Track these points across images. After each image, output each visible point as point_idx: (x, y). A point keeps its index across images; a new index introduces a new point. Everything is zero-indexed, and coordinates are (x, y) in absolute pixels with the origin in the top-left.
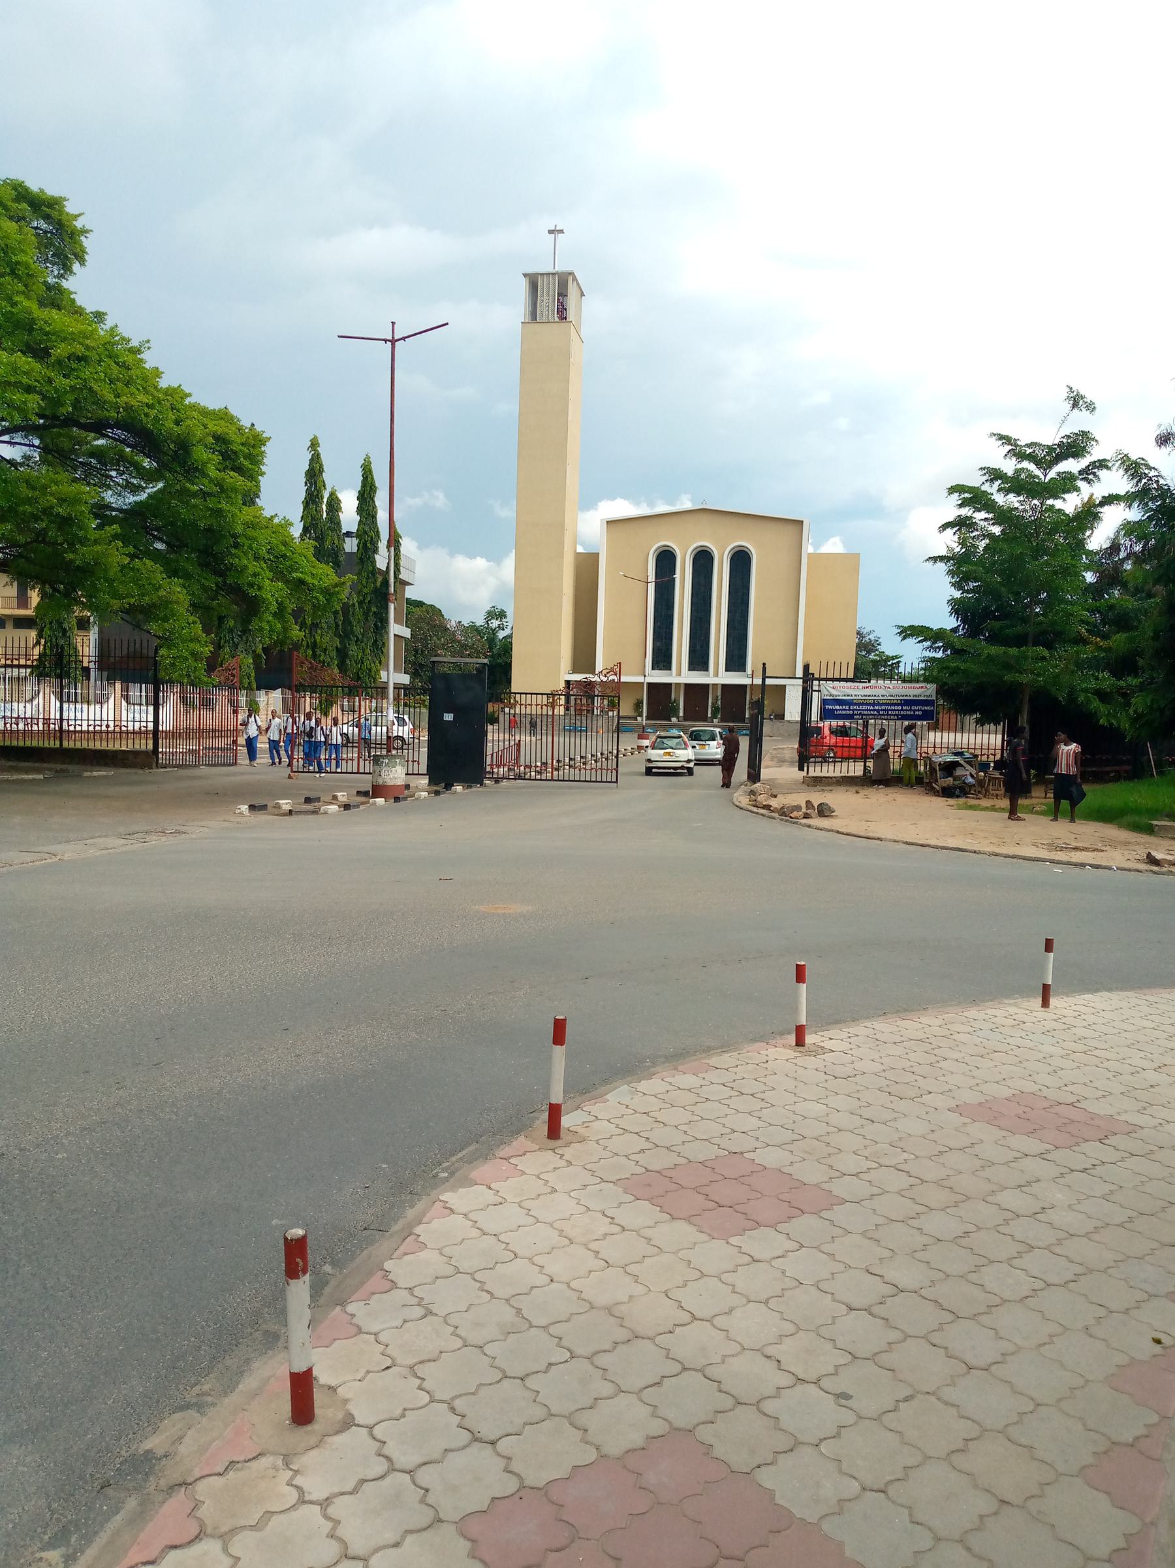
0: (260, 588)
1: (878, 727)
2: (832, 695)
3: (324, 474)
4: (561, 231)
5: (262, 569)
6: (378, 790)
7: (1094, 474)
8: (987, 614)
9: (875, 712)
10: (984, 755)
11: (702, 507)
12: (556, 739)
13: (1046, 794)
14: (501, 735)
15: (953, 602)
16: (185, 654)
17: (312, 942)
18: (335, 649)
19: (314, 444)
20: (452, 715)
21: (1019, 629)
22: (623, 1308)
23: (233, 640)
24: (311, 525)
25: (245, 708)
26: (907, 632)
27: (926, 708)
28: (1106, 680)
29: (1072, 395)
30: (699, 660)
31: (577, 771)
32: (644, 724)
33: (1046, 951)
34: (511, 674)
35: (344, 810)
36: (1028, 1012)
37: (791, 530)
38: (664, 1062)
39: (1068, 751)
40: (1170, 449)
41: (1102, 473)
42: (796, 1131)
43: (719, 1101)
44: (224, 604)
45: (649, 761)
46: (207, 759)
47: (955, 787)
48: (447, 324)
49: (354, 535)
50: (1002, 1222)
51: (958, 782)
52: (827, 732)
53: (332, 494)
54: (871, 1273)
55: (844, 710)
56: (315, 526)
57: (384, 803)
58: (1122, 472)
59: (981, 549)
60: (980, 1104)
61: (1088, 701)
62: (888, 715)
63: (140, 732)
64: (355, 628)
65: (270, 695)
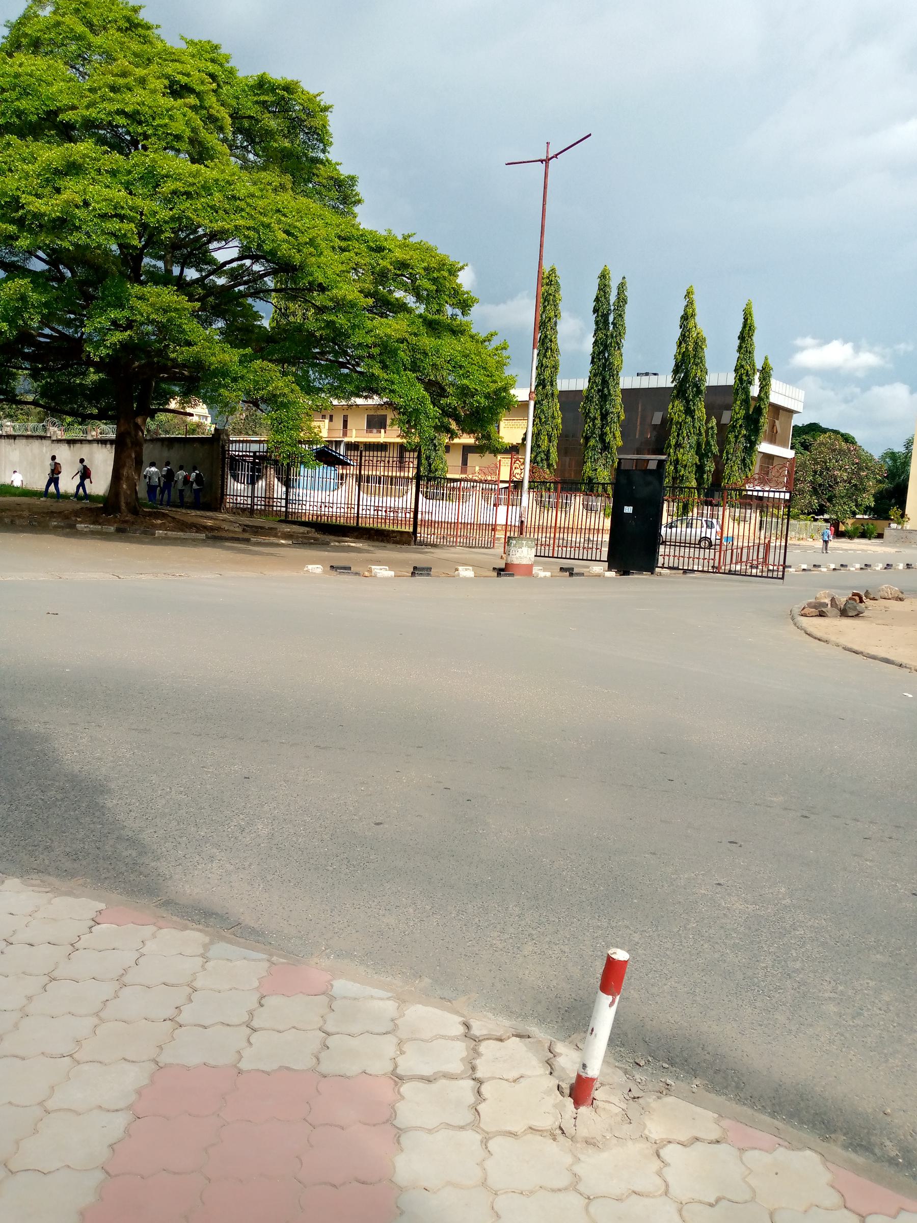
20: (632, 507)
48: (590, 135)
64: (713, 447)
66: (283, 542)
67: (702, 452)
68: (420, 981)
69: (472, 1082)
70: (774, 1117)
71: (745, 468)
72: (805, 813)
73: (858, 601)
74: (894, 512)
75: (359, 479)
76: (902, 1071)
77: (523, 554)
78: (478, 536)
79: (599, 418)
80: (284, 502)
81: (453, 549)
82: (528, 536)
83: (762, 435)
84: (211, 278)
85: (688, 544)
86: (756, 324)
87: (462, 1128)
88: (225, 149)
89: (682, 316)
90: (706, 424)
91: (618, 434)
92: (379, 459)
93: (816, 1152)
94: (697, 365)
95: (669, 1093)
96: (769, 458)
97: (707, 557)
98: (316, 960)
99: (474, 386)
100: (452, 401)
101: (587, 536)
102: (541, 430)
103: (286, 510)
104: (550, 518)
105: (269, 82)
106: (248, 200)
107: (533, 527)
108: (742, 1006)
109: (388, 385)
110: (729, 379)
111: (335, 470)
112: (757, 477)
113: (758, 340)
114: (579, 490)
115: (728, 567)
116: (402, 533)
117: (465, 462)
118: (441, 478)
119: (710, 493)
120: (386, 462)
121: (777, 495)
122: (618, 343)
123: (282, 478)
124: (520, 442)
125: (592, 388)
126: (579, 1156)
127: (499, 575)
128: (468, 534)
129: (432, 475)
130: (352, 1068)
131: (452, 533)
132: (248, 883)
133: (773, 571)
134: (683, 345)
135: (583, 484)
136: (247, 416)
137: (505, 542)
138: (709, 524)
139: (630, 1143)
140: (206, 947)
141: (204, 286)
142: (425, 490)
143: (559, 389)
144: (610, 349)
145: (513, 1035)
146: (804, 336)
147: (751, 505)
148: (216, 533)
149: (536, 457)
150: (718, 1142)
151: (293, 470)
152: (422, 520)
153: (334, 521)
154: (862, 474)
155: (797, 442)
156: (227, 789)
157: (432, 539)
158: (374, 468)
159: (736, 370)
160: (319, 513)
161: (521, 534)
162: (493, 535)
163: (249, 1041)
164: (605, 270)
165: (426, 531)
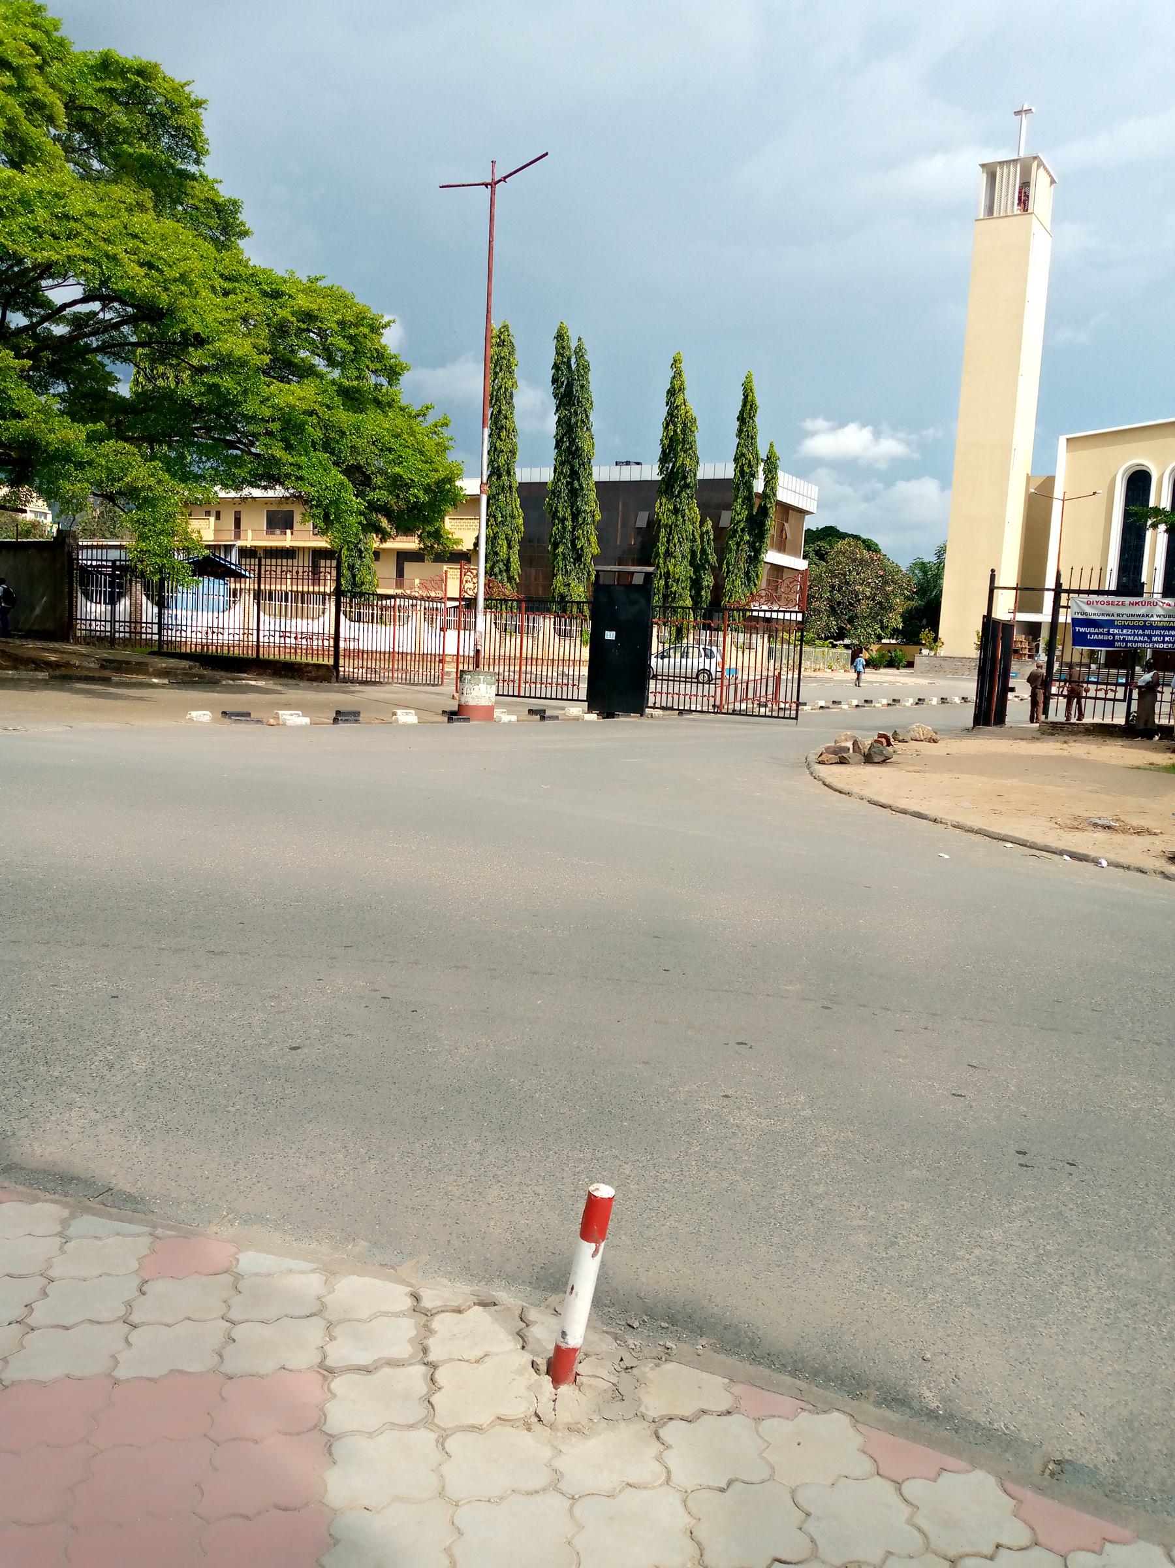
19: (676, 362)
55: (1101, 634)
66: (155, 680)
67: (697, 563)
68: (354, 1246)
69: (423, 1368)
70: (796, 1377)
71: (749, 582)
72: (826, 1004)
73: (885, 744)
74: (926, 635)
75: (258, 595)
76: (943, 1307)
77: (481, 693)
78: (421, 670)
79: (570, 518)
80: (156, 627)
81: (388, 688)
82: (486, 668)
83: (768, 541)
84: (45, 325)
85: (686, 679)
86: (758, 402)
87: (411, 1426)
88: (58, 149)
89: (669, 390)
90: (700, 527)
91: (593, 539)
92: (284, 568)
93: (844, 1412)
94: (685, 452)
95: (670, 1358)
96: (778, 569)
97: (706, 693)
98: (216, 1229)
99: (409, 476)
100: (380, 495)
101: (561, 668)
102: (497, 532)
103: (160, 638)
104: (513, 647)
105: (117, 62)
106: (87, 220)
107: (492, 657)
108: (755, 1244)
109: (293, 470)
110: (728, 471)
111: (225, 584)
112: (763, 593)
113: (761, 420)
114: (549, 611)
115: (731, 707)
116: (318, 667)
117: (400, 573)
118: (369, 594)
119: (708, 615)
120: (294, 573)
121: (787, 616)
122: (583, 421)
123: (153, 595)
124: (471, 547)
125: (559, 480)
126: (561, 1447)
127: (450, 720)
128: (409, 668)
129: (358, 590)
130: (267, 1365)
131: (387, 666)
132: (121, 1136)
133: (785, 709)
134: (671, 427)
135: (554, 602)
136: (102, 513)
137: (457, 678)
138: (708, 652)
139: (623, 1424)
140: (65, 1223)
141: (35, 337)
142: (348, 609)
143: (519, 480)
144: (576, 431)
145: (475, 1304)
146: (814, 416)
147: (757, 628)
148: (63, 671)
149: (492, 568)
150: (729, 1413)
151: (168, 584)
152: (345, 650)
153: (226, 652)
154: (887, 589)
155: (810, 549)
156: (88, 1012)
157: (361, 673)
158: (279, 580)
159: (736, 460)
160: (204, 641)
161: (478, 666)
162: (441, 668)
163: (127, 1342)
164: (561, 328)
165: (351, 664)
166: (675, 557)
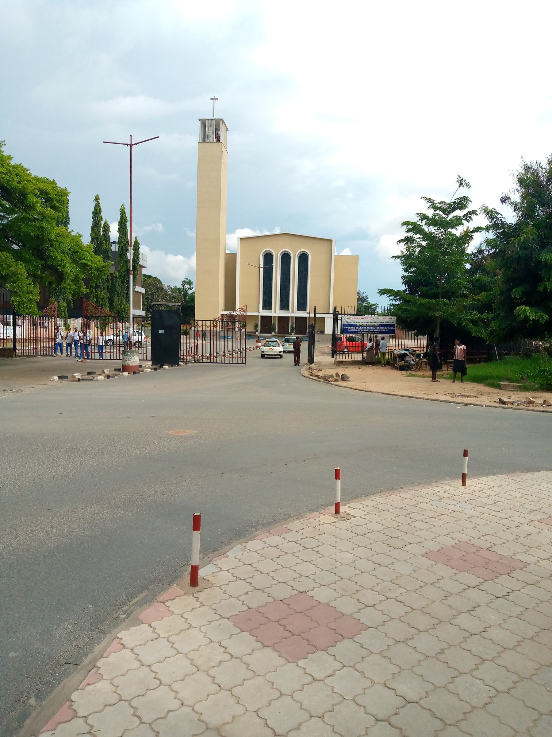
0: (64, 267)
1: (369, 337)
2: (347, 322)
3: (101, 213)
4: (217, 99)
5: (66, 258)
6: (125, 368)
7: (470, 217)
8: (420, 284)
9: (367, 330)
10: (418, 350)
11: (285, 233)
12: (215, 342)
13: (448, 369)
14: (191, 341)
15: (404, 277)
16: (25, 299)
17: (75, 454)
18: (107, 298)
19: (97, 199)
20: (163, 330)
21: (435, 291)
22: (228, 727)
23: (56, 294)
24: (95, 236)
25: (62, 327)
26: (383, 292)
27: (391, 328)
28: (476, 315)
29: (460, 180)
30: (284, 305)
31: (226, 358)
32: (259, 335)
33: (464, 456)
34: (195, 311)
35: (107, 378)
36: (455, 488)
37: (326, 244)
38: (262, 528)
39: (460, 348)
40: (507, 205)
41: (474, 217)
42: (337, 574)
43: (293, 554)
44: (49, 277)
45: (263, 352)
46: (41, 352)
47: (405, 366)
49: (117, 243)
50: (463, 640)
51: (407, 363)
52: (345, 339)
53: (105, 223)
54: (388, 687)
55: (353, 329)
56: (97, 239)
57: (128, 375)
58: (485, 215)
59: (417, 252)
60: (438, 551)
61: (467, 325)
62: (373, 331)
63: (7, 339)
65: (75, 321)
166: (100, 288)
